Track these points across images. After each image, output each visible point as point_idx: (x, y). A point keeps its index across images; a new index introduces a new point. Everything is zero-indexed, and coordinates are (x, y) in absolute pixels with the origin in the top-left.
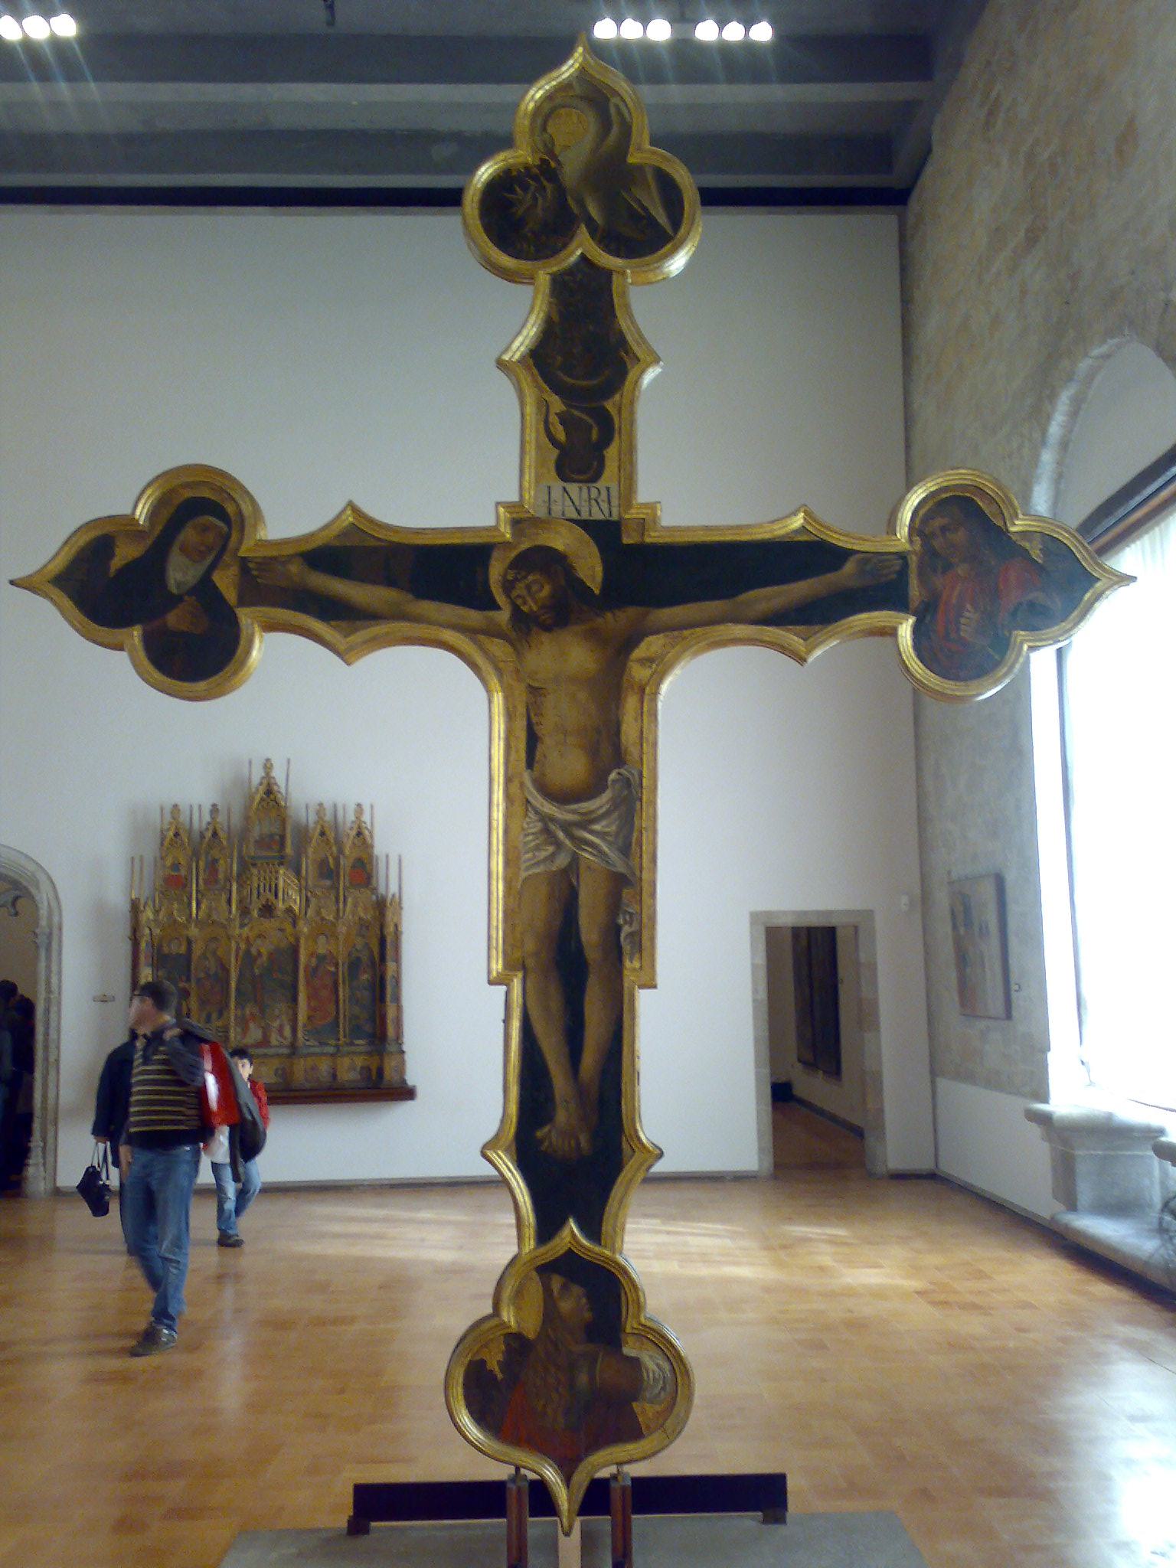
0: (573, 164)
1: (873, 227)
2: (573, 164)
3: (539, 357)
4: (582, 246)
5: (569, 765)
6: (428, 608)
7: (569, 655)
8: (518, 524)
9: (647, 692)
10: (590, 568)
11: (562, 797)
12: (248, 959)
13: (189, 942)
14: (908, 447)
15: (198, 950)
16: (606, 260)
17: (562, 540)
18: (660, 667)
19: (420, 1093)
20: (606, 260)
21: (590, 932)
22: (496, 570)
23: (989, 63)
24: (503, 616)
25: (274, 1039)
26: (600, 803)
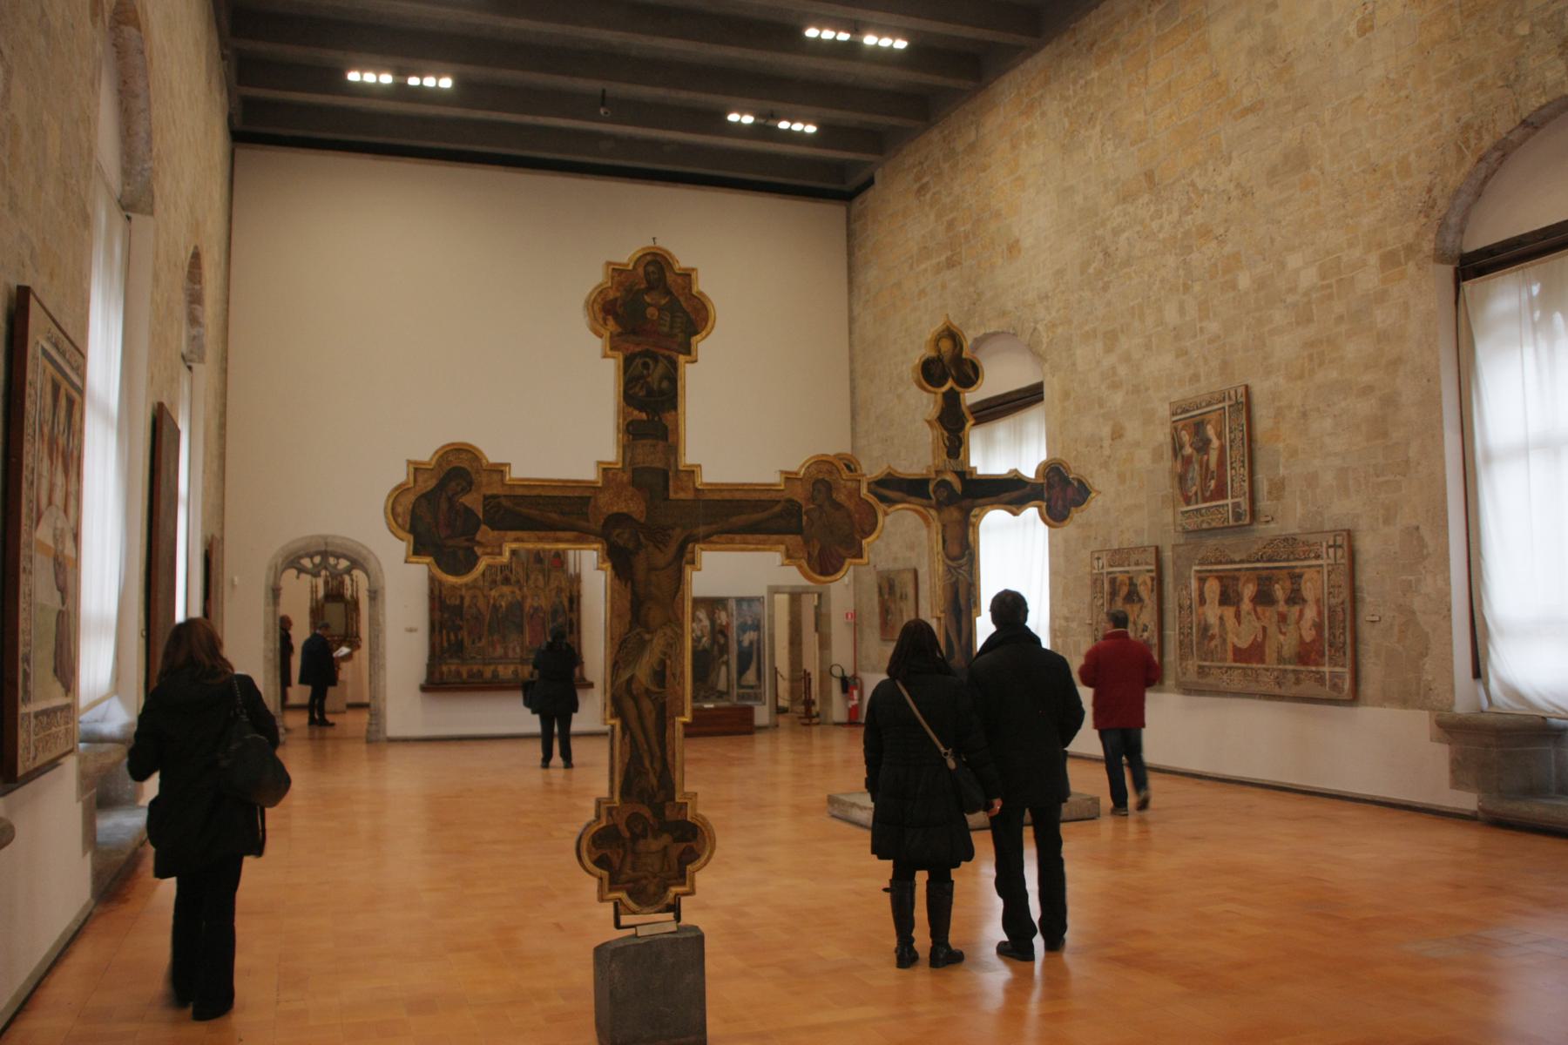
0: (947, 357)
1: (832, 213)
2: (947, 357)
3: (940, 419)
4: (950, 384)
5: (955, 550)
6: (912, 499)
7: (954, 514)
8: (938, 472)
9: (976, 527)
10: (957, 486)
11: (954, 559)
12: (496, 608)
13: (462, 598)
14: (851, 332)
15: (467, 602)
16: (958, 389)
17: (949, 477)
18: (979, 517)
19: (419, 693)
20: (958, 389)
21: (962, 602)
22: (931, 487)
23: (921, 163)
24: (934, 502)
25: (511, 654)
26: (963, 561)
